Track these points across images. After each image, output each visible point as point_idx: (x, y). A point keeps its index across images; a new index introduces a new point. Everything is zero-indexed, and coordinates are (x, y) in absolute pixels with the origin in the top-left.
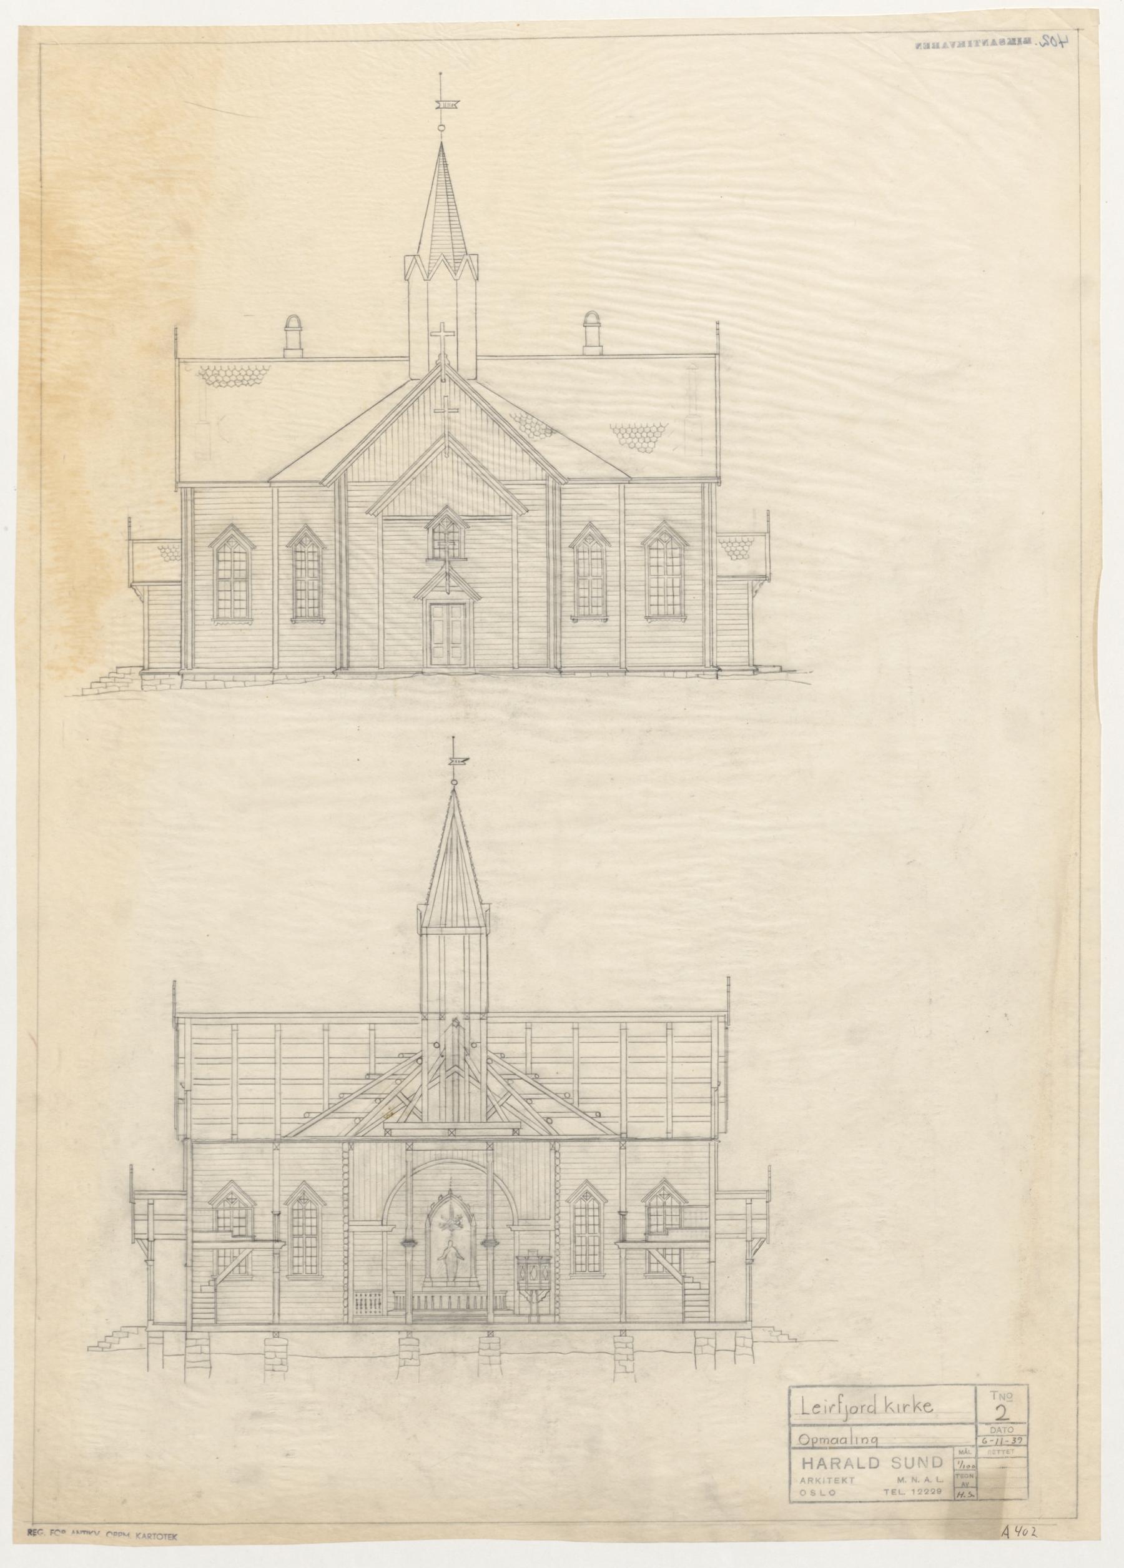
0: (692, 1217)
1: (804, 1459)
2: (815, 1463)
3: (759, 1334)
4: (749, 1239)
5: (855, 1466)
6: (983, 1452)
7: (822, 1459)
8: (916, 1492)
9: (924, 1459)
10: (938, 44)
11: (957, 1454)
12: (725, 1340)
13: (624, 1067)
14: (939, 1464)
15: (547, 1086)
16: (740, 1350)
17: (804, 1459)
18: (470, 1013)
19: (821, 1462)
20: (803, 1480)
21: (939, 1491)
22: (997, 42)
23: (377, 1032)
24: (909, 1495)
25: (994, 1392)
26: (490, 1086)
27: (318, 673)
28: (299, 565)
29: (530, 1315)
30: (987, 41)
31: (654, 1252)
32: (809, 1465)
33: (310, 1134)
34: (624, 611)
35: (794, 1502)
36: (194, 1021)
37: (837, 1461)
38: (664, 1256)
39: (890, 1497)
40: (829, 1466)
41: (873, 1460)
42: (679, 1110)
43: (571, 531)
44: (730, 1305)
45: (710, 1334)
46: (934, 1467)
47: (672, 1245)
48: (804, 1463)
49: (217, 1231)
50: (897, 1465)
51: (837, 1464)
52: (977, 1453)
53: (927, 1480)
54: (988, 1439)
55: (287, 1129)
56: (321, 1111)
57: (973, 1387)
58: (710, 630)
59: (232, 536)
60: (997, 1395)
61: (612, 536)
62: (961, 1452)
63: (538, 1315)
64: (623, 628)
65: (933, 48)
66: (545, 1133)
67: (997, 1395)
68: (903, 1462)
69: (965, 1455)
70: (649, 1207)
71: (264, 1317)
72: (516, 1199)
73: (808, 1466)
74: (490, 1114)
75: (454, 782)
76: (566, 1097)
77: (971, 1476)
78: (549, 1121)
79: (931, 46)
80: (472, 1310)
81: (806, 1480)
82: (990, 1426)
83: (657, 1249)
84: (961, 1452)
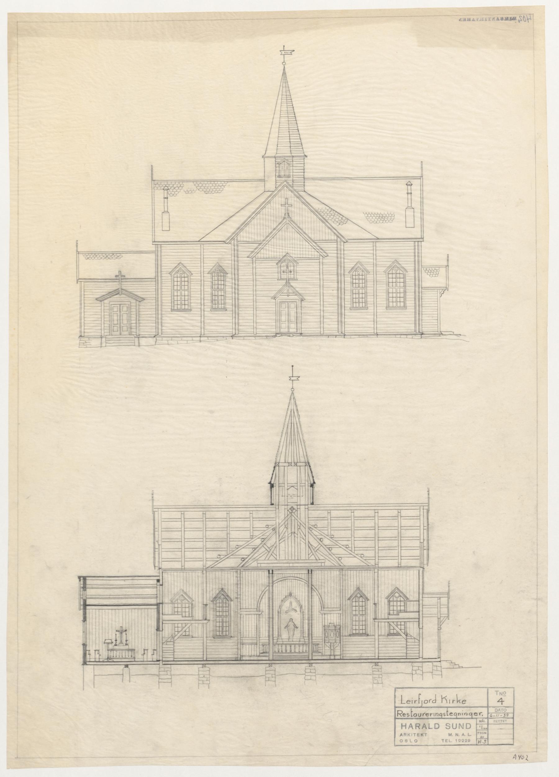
0: (412, 607)
1: (402, 724)
2: (408, 726)
3: (444, 664)
4: (439, 617)
5: (428, 728)
6: (491, 721)
7: (424, 724)
8: (458, 741)
9: (462, 725)
10: (470, 19)
11: (478, 722)
12: (427, 667)
13: (399, 531)
14: (469, 727)
15: (339, 542)
16: (435, 672)
17: (402, 724)
18: (300, 505)
19: (411, 726)
20: (401, 735)
21: (469, 741)
22: (500, 19)
23: (206, 515)
24: (454, 742)
25: (497, 691)
26: (310, 541)
27: (223, 337)
28: (354, 282)
29: (330, 655)
30: (461, 19)
31: (392, 623)
32: (404, 727)
33: (221, 566)
34: (375, 305)
35: (397, 746)
36: (162, 510)
37: (418, 725)
38: (397, 625)
39: (444, 743)
40: (414, 727)
41: (468, 725)
42: (188, 554)
43: (349, 265)
44: (429, 650)
45: (420, 664)
46: (466, 728)
47: (400, 620)
48: (402, 726)
49: (174, 614)
50: (448, 727)
51: (418, 727)
52: (488, 722)
53: (463, 735)
54: (493, 714)
55: (209, 564)
56: (226, 554)
57: (487, 689)
58: (418, 313)
59: (358, 267)
60: (498, 693)
61: (370, 268)
62: (480, 721)
63: (334, 656)
64: (375, 314)
65: (468, 20)
66: (337, 565)
67: (498, 693)
68: (451, 725)
69: (483, 723)
70: (389, 601)
71: (402, 655)
72: (322, 597)
73: (404, 728)
74: (310, 556)
75: (293, 390)
76: (347, 547)
77: (485, 733)
78: (339, 558)
79: (467, 20)
80: (293, 653)
81: (403, 734)
82: (494, 708)
83: (393, 622)
84: (480, 721)
